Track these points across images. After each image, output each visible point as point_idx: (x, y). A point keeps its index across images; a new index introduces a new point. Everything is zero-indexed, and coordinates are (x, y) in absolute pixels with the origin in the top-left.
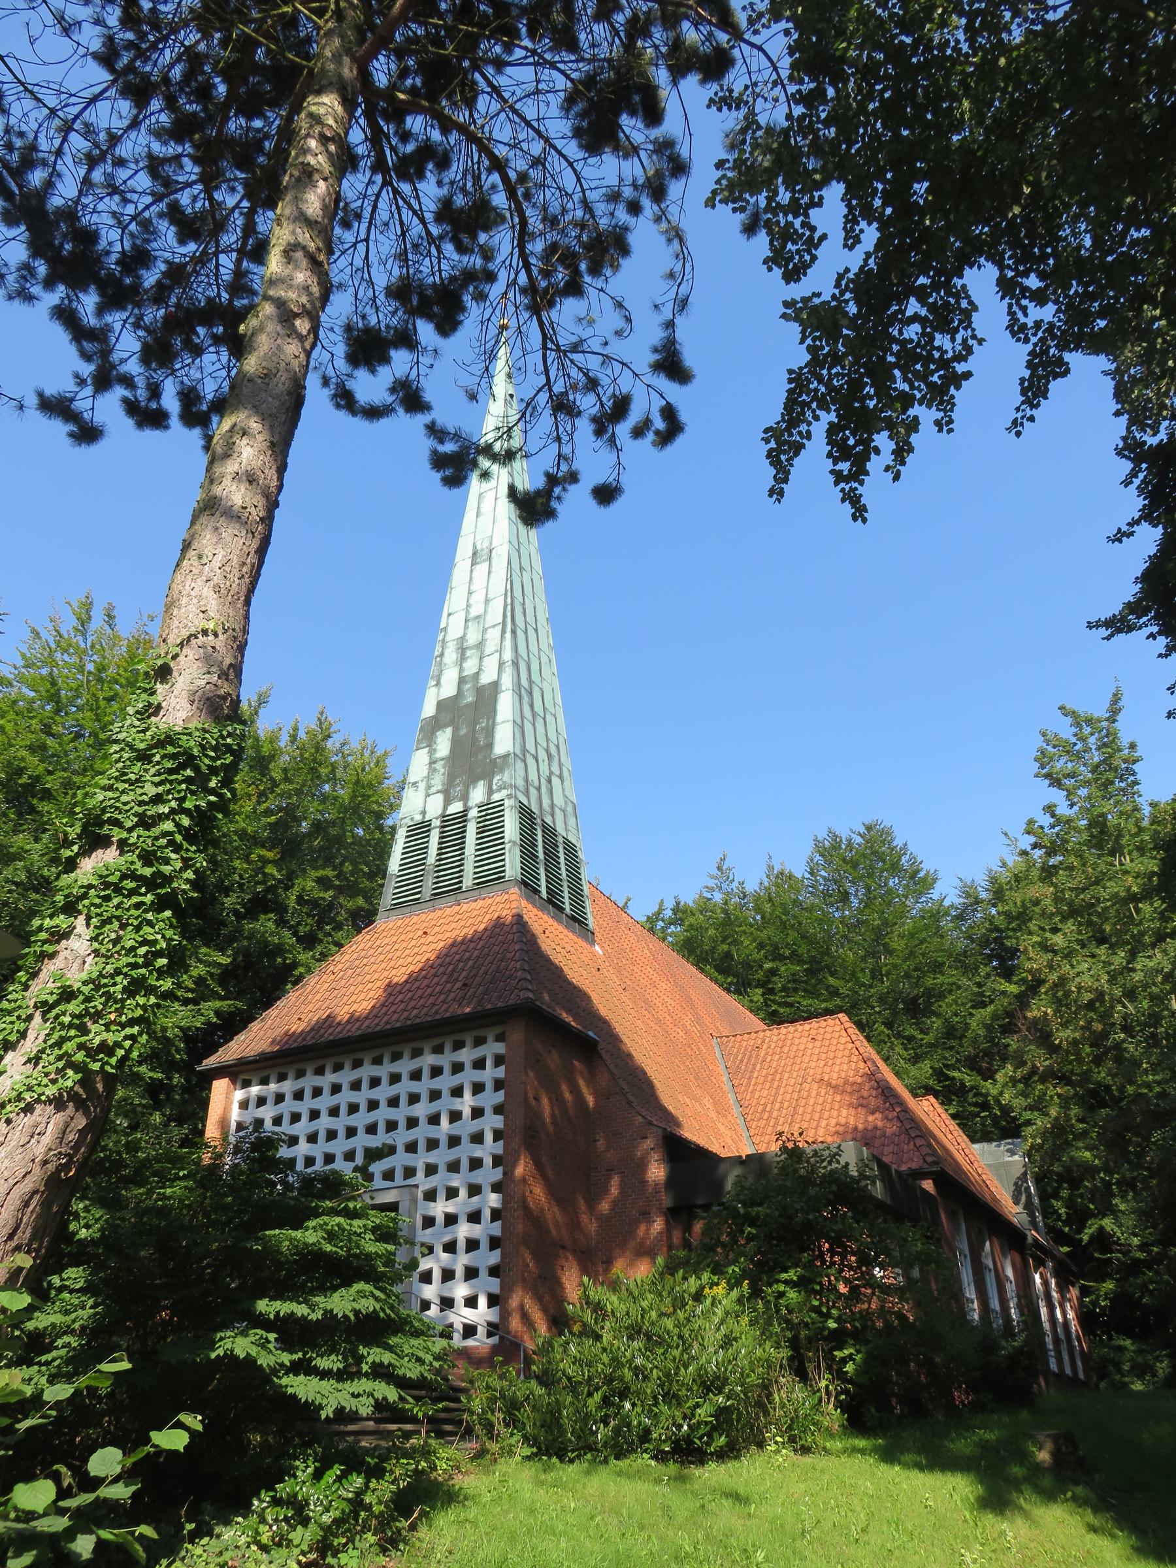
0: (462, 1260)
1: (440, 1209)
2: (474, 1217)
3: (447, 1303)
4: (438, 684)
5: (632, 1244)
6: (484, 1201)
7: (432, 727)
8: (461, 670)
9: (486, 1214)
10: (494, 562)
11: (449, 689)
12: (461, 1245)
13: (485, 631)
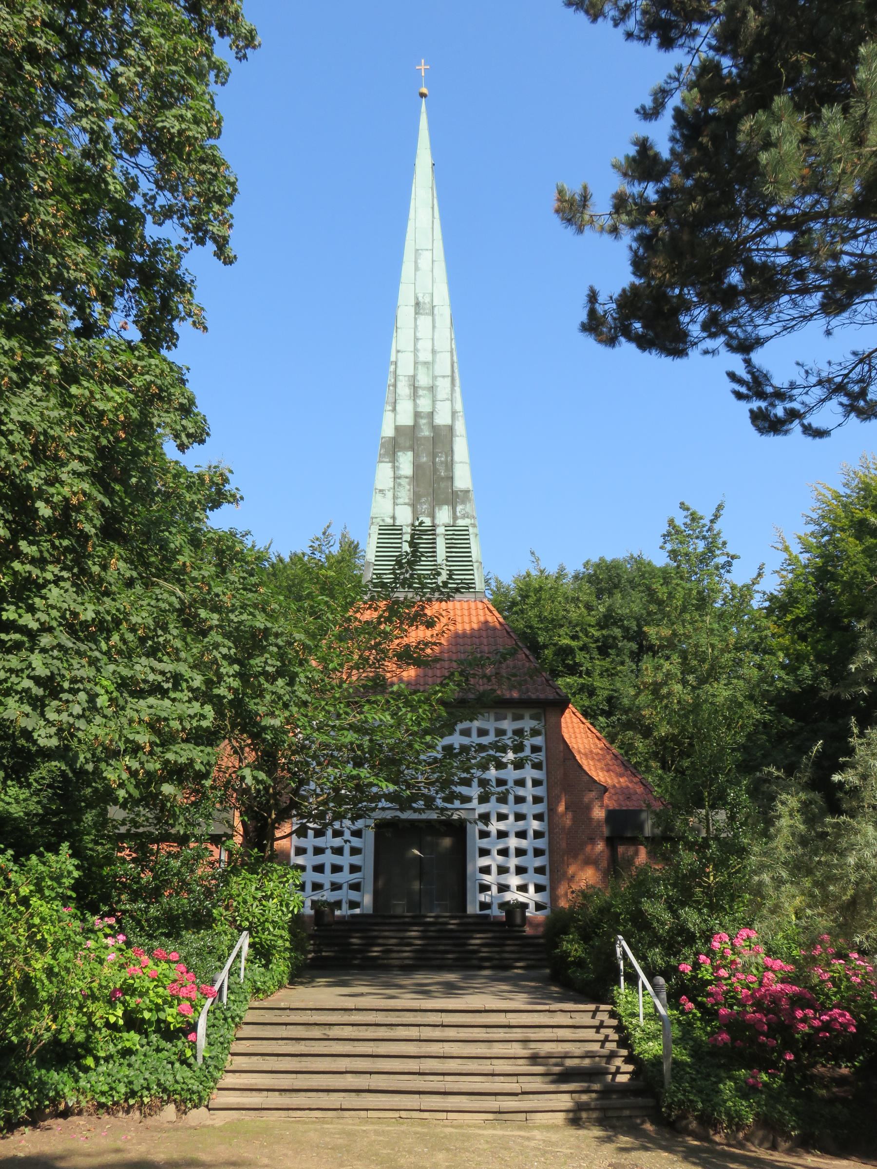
0: (513, 862)
1: (495, 826)
2: (521, 835)
3: (503, 888)
4: (394, 410)
5: (581, 857)
6: (529, 825)
7: (392, 448)
8: (415, 405)
9: (531, 833)
10: (437, 318)
11: (406, 419)
12: (512, 851)
13: (435, 378)
